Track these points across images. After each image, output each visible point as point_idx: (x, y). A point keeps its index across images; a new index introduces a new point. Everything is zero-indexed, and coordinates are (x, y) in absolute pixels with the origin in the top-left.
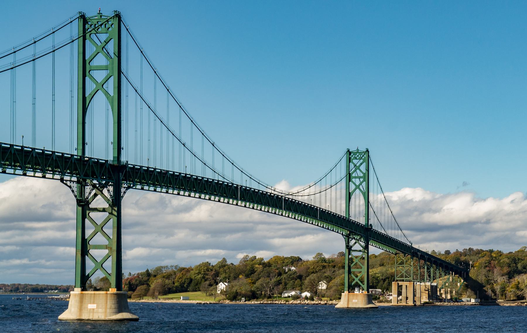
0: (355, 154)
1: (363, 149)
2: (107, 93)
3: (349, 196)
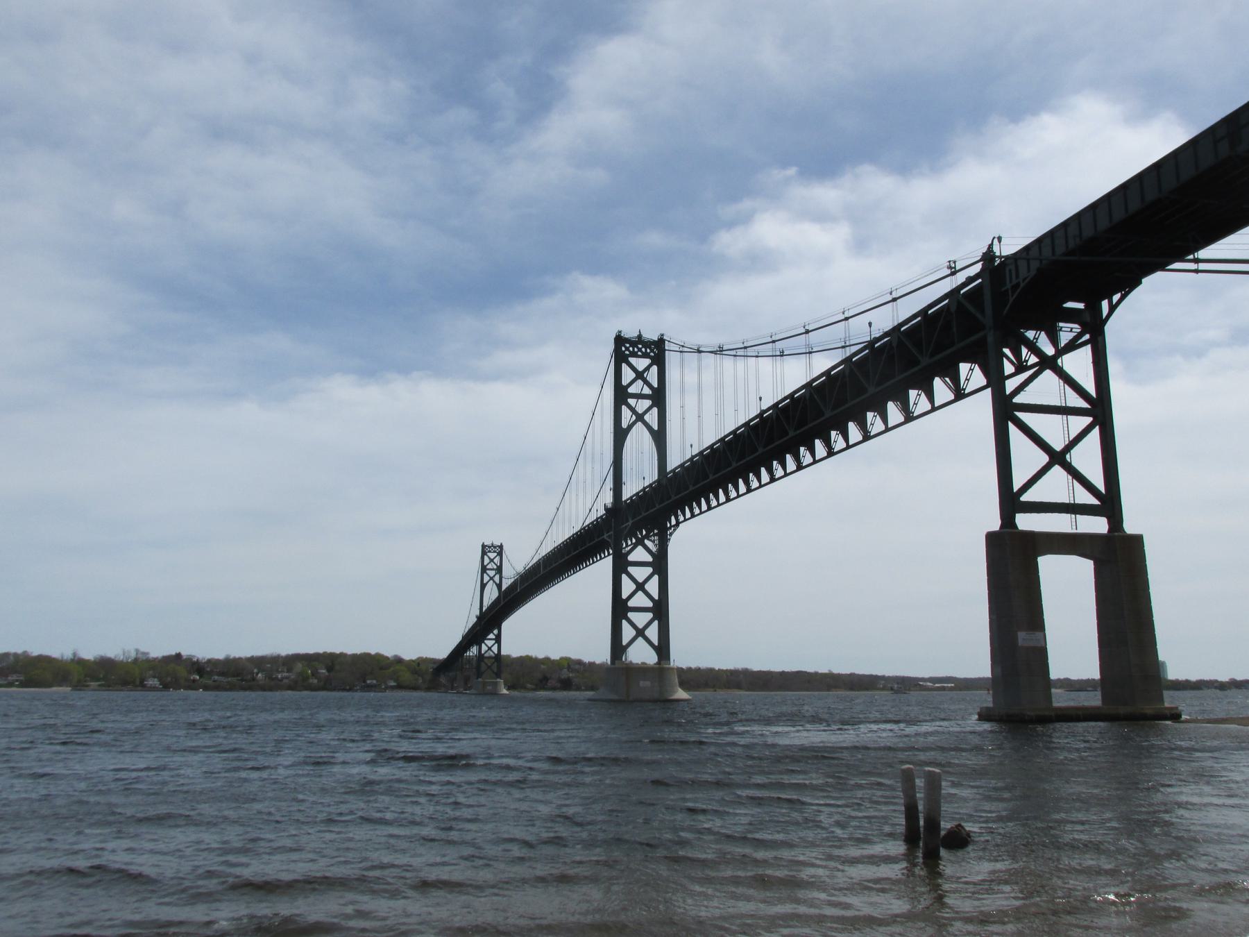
0: (489, 547)
1: (497, 543)
2: (494, 581)
3: (483, 586)
